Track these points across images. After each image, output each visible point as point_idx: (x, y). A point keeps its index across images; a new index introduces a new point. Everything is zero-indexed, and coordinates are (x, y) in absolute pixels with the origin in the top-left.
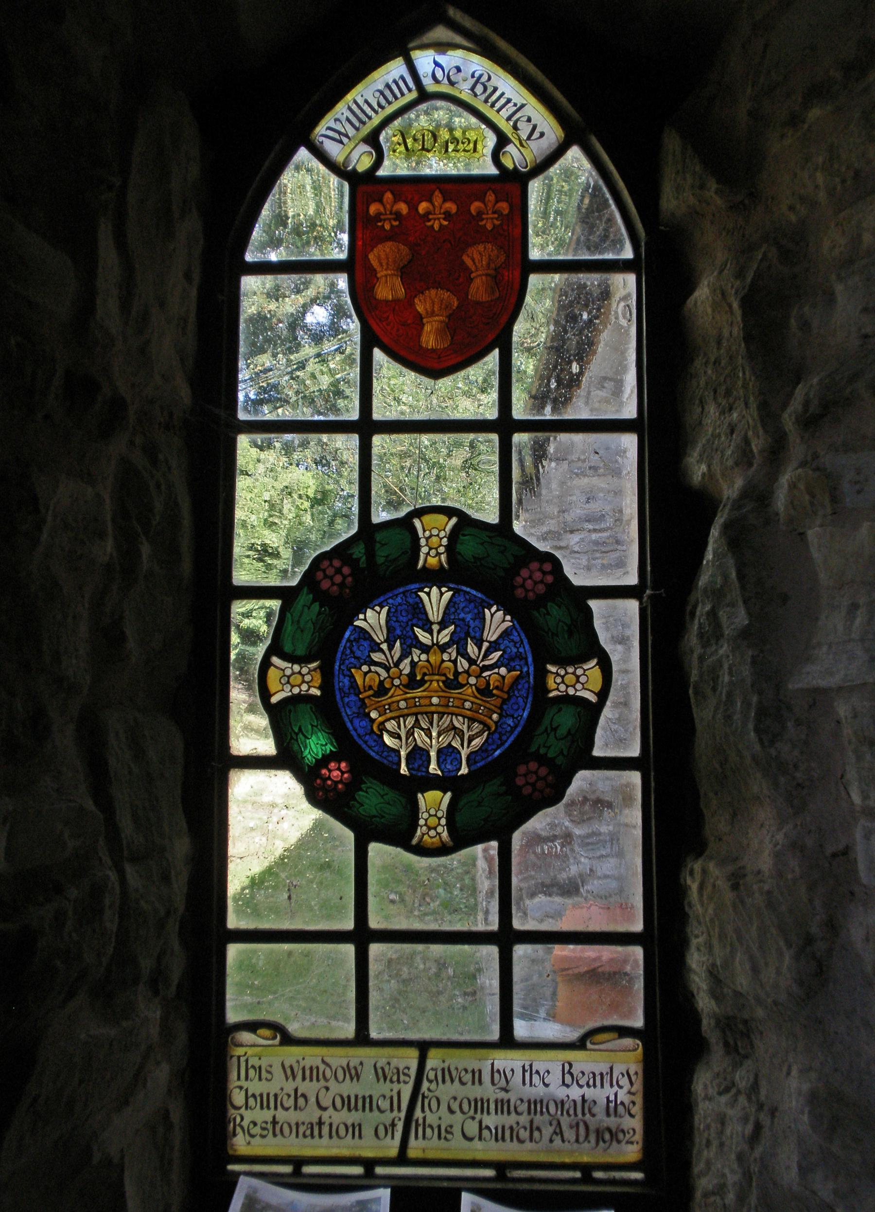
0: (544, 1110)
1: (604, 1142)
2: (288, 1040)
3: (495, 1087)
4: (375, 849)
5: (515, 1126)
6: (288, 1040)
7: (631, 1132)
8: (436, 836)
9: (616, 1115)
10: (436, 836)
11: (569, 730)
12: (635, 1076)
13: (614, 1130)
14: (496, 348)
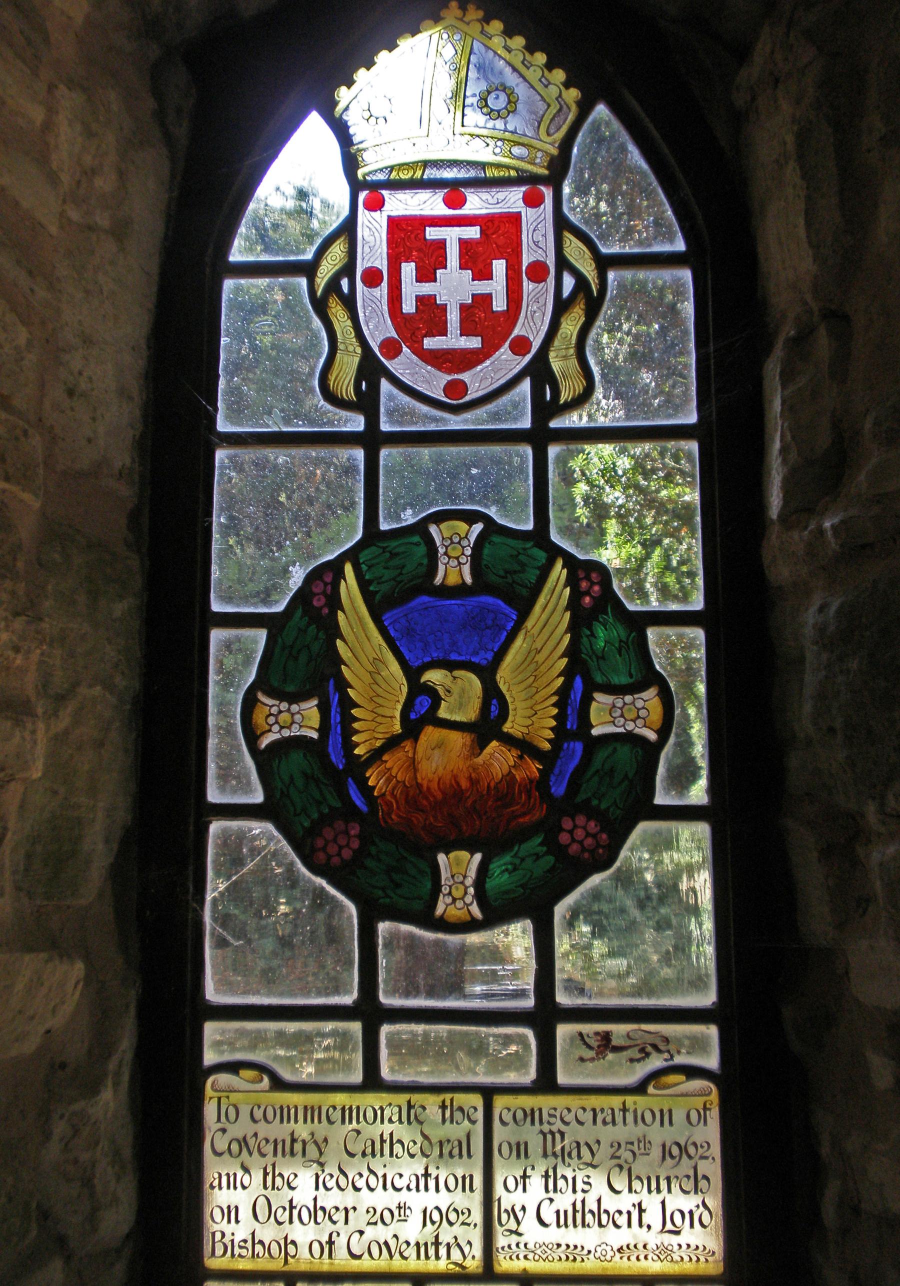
0: (379, 1112)
1: (672, 1157)
2: (278, 1084)
3: (264, 1192)
4: (262, 635)
5: (694, 1209)
6: (278, 1084)
7: (705, 1145)
8: (463, 908)
9: (452, 1122)
10: (463, 908)
11: (595, 637)
12: (214, 1185)
13: (683, 1144)
14: (473, 583)
